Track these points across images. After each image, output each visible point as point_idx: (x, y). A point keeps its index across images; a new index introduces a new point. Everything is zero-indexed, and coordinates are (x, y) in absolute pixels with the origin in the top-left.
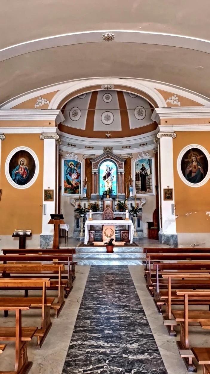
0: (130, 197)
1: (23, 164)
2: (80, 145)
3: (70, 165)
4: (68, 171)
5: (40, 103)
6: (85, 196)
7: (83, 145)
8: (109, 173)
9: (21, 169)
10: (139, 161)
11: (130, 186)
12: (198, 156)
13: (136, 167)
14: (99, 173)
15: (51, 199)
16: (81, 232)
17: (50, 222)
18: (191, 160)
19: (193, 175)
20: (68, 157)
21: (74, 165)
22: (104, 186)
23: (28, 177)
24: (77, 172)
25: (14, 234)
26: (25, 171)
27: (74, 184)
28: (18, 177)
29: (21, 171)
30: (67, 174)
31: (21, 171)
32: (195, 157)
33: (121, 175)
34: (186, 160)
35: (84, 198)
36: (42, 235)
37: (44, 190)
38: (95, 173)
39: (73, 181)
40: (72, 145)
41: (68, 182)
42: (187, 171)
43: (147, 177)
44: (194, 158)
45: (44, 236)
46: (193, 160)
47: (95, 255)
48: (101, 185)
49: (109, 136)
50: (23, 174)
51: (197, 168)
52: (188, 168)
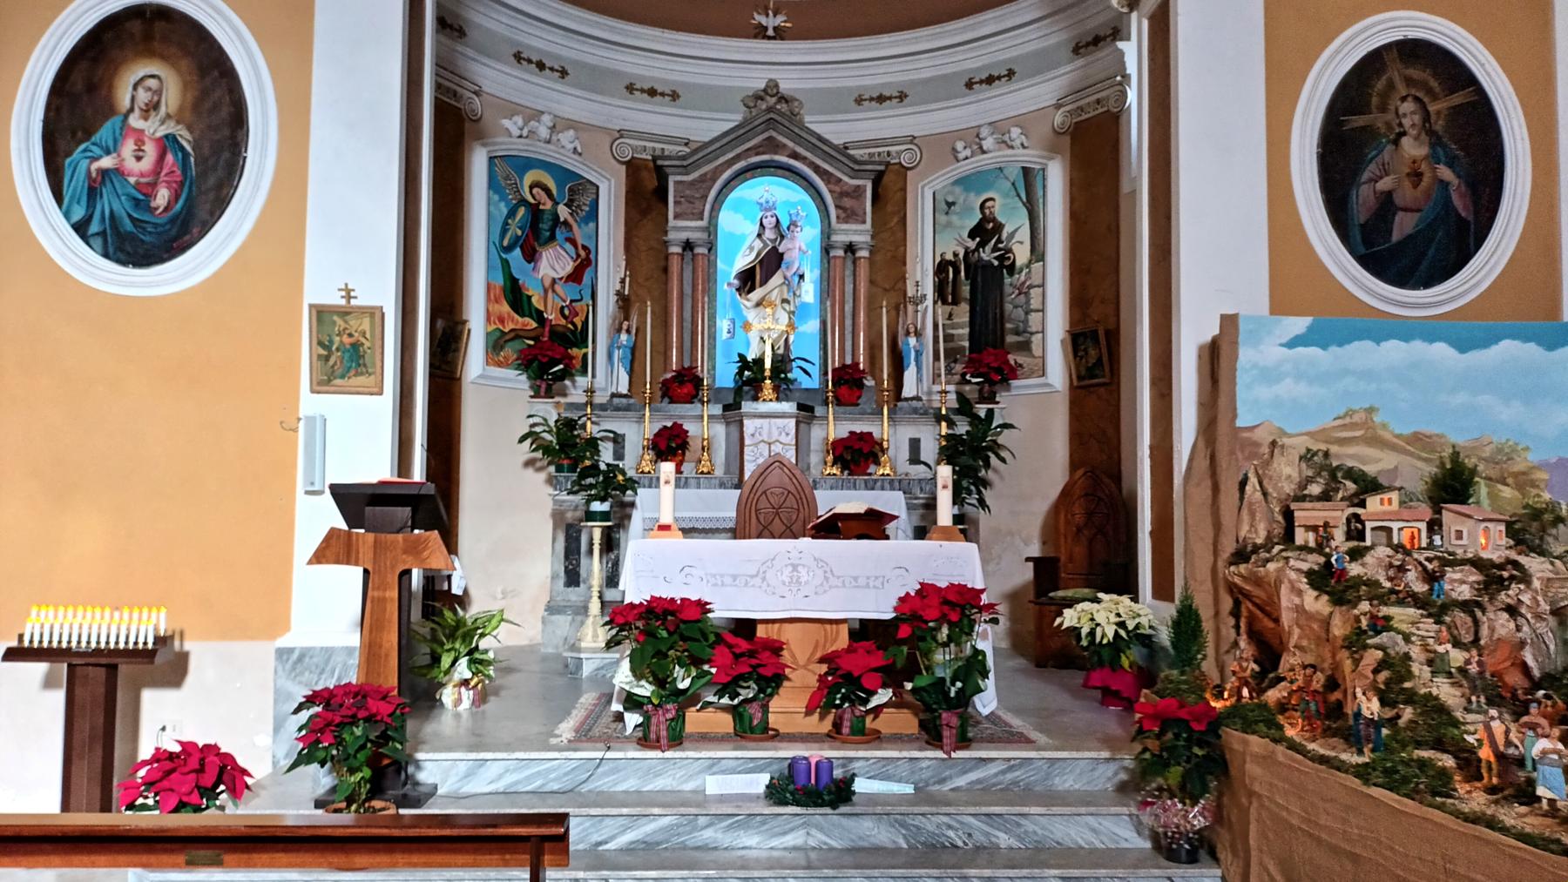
0: (907, 399)
1: (151, 108)
2: (593, 69)
3: (531, 188)
4: (515, 230)
6: (624, 389)
7: (616, 74)
8: (775, 249)
9: (140, 142)
10: (957, 182)
11: (908, 333)
12: (1435, 98)
13: (942, 218)
14: (711, 247)
15: (361, 380)
16: (590, 620)
17: (332, 550)
18: (1389, 125)
19: (1403, 225)
20: (510, 135)
21: (555, 192)
22: (745, 328)
23: (187, 200)
24: (573, 242)
25: (21, 637)
26: (170, 158)
27: (551, 316)
28: (109, 202)
29: (139, 159)
30: (505, 243)
31: (139, 159)
32: (1417, 99)
33: (849, 264)
34: (1359, 121)
35: (616, 400)
36: (291, 650)
37: (311, 306)
38: (688, 246)
39: (546, 291)
40: (541, 66)
41: (515, 295)
42: (1363, 198)
43: (1007, 280)
44: (1408, 107)
45: (300, 659)
46: (1400, 125)
47: (702, 821)
48: (723, 325)
49: (775, 29)
50: (154, 185)
52: (1365, 176)
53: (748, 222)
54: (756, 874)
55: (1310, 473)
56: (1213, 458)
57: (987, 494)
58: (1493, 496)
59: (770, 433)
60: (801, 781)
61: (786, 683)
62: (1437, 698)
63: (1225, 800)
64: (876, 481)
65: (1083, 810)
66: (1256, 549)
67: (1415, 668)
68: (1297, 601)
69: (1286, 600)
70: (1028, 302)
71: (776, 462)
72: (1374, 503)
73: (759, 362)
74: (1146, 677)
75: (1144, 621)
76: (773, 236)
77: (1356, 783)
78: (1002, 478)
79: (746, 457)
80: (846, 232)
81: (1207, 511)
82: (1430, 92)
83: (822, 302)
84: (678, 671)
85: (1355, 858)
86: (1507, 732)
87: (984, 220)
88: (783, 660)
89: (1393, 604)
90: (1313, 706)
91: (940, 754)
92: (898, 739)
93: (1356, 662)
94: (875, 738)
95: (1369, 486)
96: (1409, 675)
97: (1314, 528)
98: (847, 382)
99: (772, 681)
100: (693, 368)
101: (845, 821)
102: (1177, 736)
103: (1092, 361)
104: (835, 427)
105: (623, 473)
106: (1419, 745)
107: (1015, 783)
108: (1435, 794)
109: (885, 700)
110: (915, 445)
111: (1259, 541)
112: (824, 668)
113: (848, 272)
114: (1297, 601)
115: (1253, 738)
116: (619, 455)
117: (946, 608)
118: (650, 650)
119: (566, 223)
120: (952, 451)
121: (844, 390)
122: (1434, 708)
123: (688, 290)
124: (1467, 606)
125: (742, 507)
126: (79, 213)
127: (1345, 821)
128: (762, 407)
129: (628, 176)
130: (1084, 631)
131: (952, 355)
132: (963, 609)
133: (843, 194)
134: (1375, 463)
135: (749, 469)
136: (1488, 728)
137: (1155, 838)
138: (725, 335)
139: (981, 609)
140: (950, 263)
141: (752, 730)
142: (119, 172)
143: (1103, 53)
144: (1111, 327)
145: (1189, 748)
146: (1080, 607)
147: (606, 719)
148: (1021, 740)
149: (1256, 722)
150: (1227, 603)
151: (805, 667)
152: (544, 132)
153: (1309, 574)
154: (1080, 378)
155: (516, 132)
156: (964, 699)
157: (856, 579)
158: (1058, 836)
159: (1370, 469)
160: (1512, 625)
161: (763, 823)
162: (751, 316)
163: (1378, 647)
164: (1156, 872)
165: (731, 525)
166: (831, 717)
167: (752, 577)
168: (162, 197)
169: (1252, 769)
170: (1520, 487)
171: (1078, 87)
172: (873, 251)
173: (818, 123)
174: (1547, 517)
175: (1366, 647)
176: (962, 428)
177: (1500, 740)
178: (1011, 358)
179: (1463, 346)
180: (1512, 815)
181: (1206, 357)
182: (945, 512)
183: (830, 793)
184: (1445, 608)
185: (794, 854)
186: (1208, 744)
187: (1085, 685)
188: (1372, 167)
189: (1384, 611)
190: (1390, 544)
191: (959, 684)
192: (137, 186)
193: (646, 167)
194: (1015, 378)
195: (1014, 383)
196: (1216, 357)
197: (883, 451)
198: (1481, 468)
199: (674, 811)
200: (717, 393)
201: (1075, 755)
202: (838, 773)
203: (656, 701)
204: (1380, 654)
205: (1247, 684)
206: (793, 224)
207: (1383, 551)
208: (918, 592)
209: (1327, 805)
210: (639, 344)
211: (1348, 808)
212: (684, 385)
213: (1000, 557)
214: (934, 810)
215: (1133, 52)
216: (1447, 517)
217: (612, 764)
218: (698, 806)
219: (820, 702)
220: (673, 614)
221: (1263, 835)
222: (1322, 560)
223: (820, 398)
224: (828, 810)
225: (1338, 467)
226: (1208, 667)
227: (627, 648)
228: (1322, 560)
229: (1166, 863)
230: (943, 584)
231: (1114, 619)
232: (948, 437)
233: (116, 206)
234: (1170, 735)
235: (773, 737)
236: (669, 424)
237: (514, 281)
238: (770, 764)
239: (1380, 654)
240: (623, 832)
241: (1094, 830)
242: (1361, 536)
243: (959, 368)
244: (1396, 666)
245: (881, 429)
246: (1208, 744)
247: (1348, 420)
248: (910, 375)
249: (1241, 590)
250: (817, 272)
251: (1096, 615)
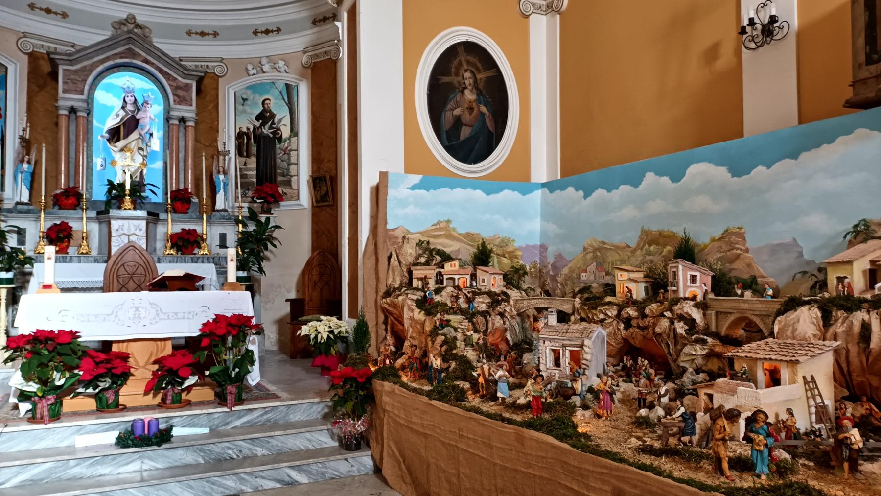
0: (218, 211)
6: (25, 198)
8: (133, 117)
10: (248, 88)
11: (219, 172)
12: (479, 72)
13: (240, 107)
14: (89, 112)
18: (459, 82)
19: (465, 132)
22: (120, 165)
32: (472, 72)
33: (182, 129)
34: (445, 79)
35: (20, 207)
38: (73, 110)
42: (448, 118)
43: (278, 146)
44: (467, 75)
46: (464, 83)
48: (98, 161)
51: (475, 111)
52: (449, 107)
53: (116, 99)
54: (107, 489)
55: (421, 252)
56: (376, 245)
57: (264, 264)
58: (499, 263)
59: (129, 229)
60: (138, 432)
61: (131, 378)
62: (466, 357)
63: (374, 416)
64: (198, 258)
65: (303, 430)
66: (395, 289)
67: (458, 344)
68: (411, 314)
69: (406, 314)
70: (289, 159)
71: (131, 246)
72: (448, 266)
73: (122, 185)
74: (342, 358)
75: (343, 329)
76: (132, 109)
77: (425, 399)
78: (275, 256)
79: (112, 244)
80: (179, 110)
81: (373, 272)
82: (477, 69)
83: (164, 151)
84: (56, 375)
85: (426, 435)
86: (490, 369)
87: (264, 111)
88: (129, 364)
89: (451, 314)
90: (415, 365)
91: (226, 409)
92: (201, 404)
93: (433, 342)
94: (188, 404)
95: (447, 258)
96: (455, 347)
97: (421, 279)
98: (180, 199)
99: (122, 376)
100: (76, 188)
101: (165, 452)
102: (352, 386)
103: (323, 193)
104: (172, 226)
105: (23, 253)
106: (457, 379)
107: (268, 420)
108: (457, 400)
109: (193, 382)
110: (223, 237)
111: (397, 286)
112: (156, 367)
113: (181, 134)
114: (411, 314)
115: (386, 384)
116: (21, 242)
117: (230, 328)
118: (35, 362)
120: (244, 241)
121: (178, 204)
122: (465, 363)
123: (73, 137)
124: (484, 314)
125: (108, 274)
127: (422, 419)
128: (123, 213)
129: (29, 62)
130: (312, 337)
131: (245, 186)
132: (240, 327)
134: (450, 247)
135: (114, 250)
136: (482, 368)
137: (340, 440)
138: (99, 168)
139: (252, 327)
140: (245, 133)
141: (108, 406)
143: (327, 27)
144: (333, 172)
145: (357, 391)
146: (310, 324)
147: (7, 409)
148: (275, 397)
149: (388, 375)
150: (382, 318)
151: (144, 367)
153: (417, 301)
154: (317, 202)
156: (241, 378)
157: (176, 314)
158: (290, 445)
159: (447, 250)
160: (502, 321)
161: (113, 460)
162: (117, 156)
163: (442, 335)
164: (339, 457)
165: (102, 285)
166: (160, 396)
167: (108, 315)
169: (386, 399)
170: (510, 258)
171: (318, 42)
172: (197, 123)
173: (161, 43)
174: (521, 272)
175: (437, 335)
176: (251, 228)
177: (487, 373)
178: (280, 189)
179: (488, 193)
180: (490, 407)
181: (374, 193)
182: (232, 274)
183: (156, 437)
184: (473, 315)
185: (133, 475)
186: (367, 389)
187: (313, 366)
188: (452, 103)
189: (447, 317)
190: (455, 287)
191: (237, 370)
193: (43, 58)
194: (282, 200)
195: (282, 203)
196: (378, 193)
197: (203, 240)
198: (494, 249)
199: (53, 459)
200: (92, 204)
201: (301, 401)
202: (162, 426)
203: (40, 394)
204: (443, 338)
205: (388, 357)
206: (146, 102)
207: (450, 289)
208: (214, 320)
209: (416, 412)
210: (37, 171)
211: (424, 412)
212: (70, 198)
213: (274, 300)
214: (220, 440)
215: (342, 26)
216: (479, 272)
217: (8, 435)
218: (69, 454)
219: (152, 388)
220: (52, 340)
221: (389, 430)
222: (423, 294)
223: (163, 208)
224: (155, 447)
225: (433, 249)
226: (372, 350)
227: (19, 362)
228: (423, 294)
229: (344, 452)
230: (229, 315)
231: (327, 329)
232: (242, 233)
234: (348, 386)
235: (122, 410)
236: (58, 222)
238: (119, 426)
239: (443, 338)
240: (16, 476)
241: (309, 440)
242: (442, 282)
243: (250, 193)
244: (450, 343)
245: (201, 228)
246: (367, 389)
247: (438, 226)
248: (220, 197)
249: (387, 310)
250: (161, 133)
251: (319, 328)
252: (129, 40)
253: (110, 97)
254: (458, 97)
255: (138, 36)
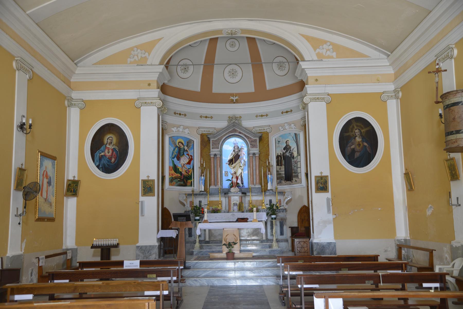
4: (175, 153)
5: (136, 57)
6: (203, 190)
8: (238, 154)
9: (109, 150)
10: (280, 136)
12: (362, 129)
13: (277, 145)
14: (221, 155)
15: (151, 194)
18: (353, 135)
19: (357, 155)
24: (188, 155)
27: (184, 173)
28: (103, 161)
29: (108, 153)
31: (108, 153)
32: (359, 129)
33: (254, 157)
34: (347, 134)
35: (201, 193)
37: (142, 180)
38: (215, 155)
40: (180, 114)
41: (175, 168)
42: (348, 150)
43: (293, 160)
44: (357, 131)
51: (361, 145)
52: (349, 145)
87: (287, 146)
119: (186, 150)
126: (97, 164)
133: (252, 141)
142: (105, 155)
152: (181, 130)
155: (175, 131)
168: (113, 160)
188: (350, 143)
192: (108, 158)
233: (104, 162)
237: (175, 165)
248: (269, 184)
252: (234, 126)
253: (228, 148)
254: (353, 141)
255: (237, 124)
